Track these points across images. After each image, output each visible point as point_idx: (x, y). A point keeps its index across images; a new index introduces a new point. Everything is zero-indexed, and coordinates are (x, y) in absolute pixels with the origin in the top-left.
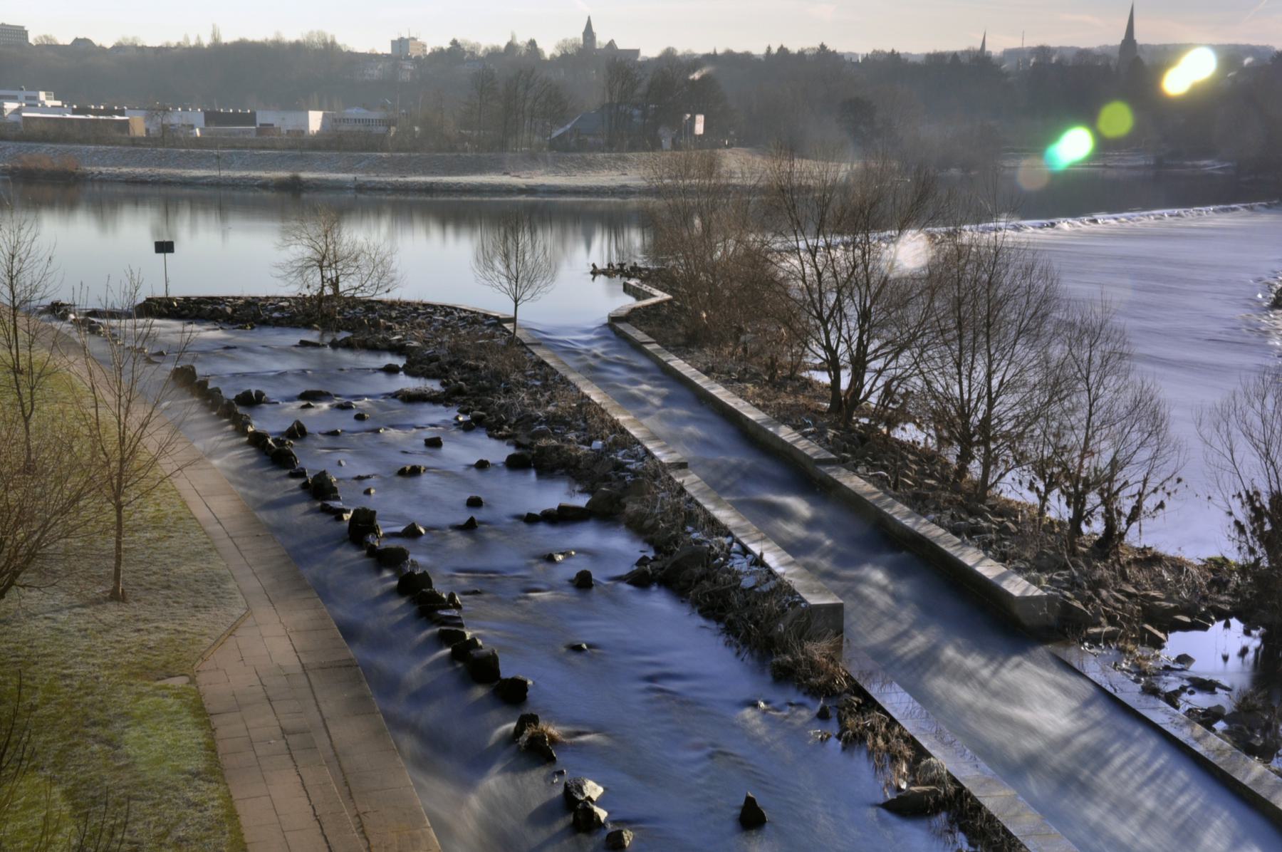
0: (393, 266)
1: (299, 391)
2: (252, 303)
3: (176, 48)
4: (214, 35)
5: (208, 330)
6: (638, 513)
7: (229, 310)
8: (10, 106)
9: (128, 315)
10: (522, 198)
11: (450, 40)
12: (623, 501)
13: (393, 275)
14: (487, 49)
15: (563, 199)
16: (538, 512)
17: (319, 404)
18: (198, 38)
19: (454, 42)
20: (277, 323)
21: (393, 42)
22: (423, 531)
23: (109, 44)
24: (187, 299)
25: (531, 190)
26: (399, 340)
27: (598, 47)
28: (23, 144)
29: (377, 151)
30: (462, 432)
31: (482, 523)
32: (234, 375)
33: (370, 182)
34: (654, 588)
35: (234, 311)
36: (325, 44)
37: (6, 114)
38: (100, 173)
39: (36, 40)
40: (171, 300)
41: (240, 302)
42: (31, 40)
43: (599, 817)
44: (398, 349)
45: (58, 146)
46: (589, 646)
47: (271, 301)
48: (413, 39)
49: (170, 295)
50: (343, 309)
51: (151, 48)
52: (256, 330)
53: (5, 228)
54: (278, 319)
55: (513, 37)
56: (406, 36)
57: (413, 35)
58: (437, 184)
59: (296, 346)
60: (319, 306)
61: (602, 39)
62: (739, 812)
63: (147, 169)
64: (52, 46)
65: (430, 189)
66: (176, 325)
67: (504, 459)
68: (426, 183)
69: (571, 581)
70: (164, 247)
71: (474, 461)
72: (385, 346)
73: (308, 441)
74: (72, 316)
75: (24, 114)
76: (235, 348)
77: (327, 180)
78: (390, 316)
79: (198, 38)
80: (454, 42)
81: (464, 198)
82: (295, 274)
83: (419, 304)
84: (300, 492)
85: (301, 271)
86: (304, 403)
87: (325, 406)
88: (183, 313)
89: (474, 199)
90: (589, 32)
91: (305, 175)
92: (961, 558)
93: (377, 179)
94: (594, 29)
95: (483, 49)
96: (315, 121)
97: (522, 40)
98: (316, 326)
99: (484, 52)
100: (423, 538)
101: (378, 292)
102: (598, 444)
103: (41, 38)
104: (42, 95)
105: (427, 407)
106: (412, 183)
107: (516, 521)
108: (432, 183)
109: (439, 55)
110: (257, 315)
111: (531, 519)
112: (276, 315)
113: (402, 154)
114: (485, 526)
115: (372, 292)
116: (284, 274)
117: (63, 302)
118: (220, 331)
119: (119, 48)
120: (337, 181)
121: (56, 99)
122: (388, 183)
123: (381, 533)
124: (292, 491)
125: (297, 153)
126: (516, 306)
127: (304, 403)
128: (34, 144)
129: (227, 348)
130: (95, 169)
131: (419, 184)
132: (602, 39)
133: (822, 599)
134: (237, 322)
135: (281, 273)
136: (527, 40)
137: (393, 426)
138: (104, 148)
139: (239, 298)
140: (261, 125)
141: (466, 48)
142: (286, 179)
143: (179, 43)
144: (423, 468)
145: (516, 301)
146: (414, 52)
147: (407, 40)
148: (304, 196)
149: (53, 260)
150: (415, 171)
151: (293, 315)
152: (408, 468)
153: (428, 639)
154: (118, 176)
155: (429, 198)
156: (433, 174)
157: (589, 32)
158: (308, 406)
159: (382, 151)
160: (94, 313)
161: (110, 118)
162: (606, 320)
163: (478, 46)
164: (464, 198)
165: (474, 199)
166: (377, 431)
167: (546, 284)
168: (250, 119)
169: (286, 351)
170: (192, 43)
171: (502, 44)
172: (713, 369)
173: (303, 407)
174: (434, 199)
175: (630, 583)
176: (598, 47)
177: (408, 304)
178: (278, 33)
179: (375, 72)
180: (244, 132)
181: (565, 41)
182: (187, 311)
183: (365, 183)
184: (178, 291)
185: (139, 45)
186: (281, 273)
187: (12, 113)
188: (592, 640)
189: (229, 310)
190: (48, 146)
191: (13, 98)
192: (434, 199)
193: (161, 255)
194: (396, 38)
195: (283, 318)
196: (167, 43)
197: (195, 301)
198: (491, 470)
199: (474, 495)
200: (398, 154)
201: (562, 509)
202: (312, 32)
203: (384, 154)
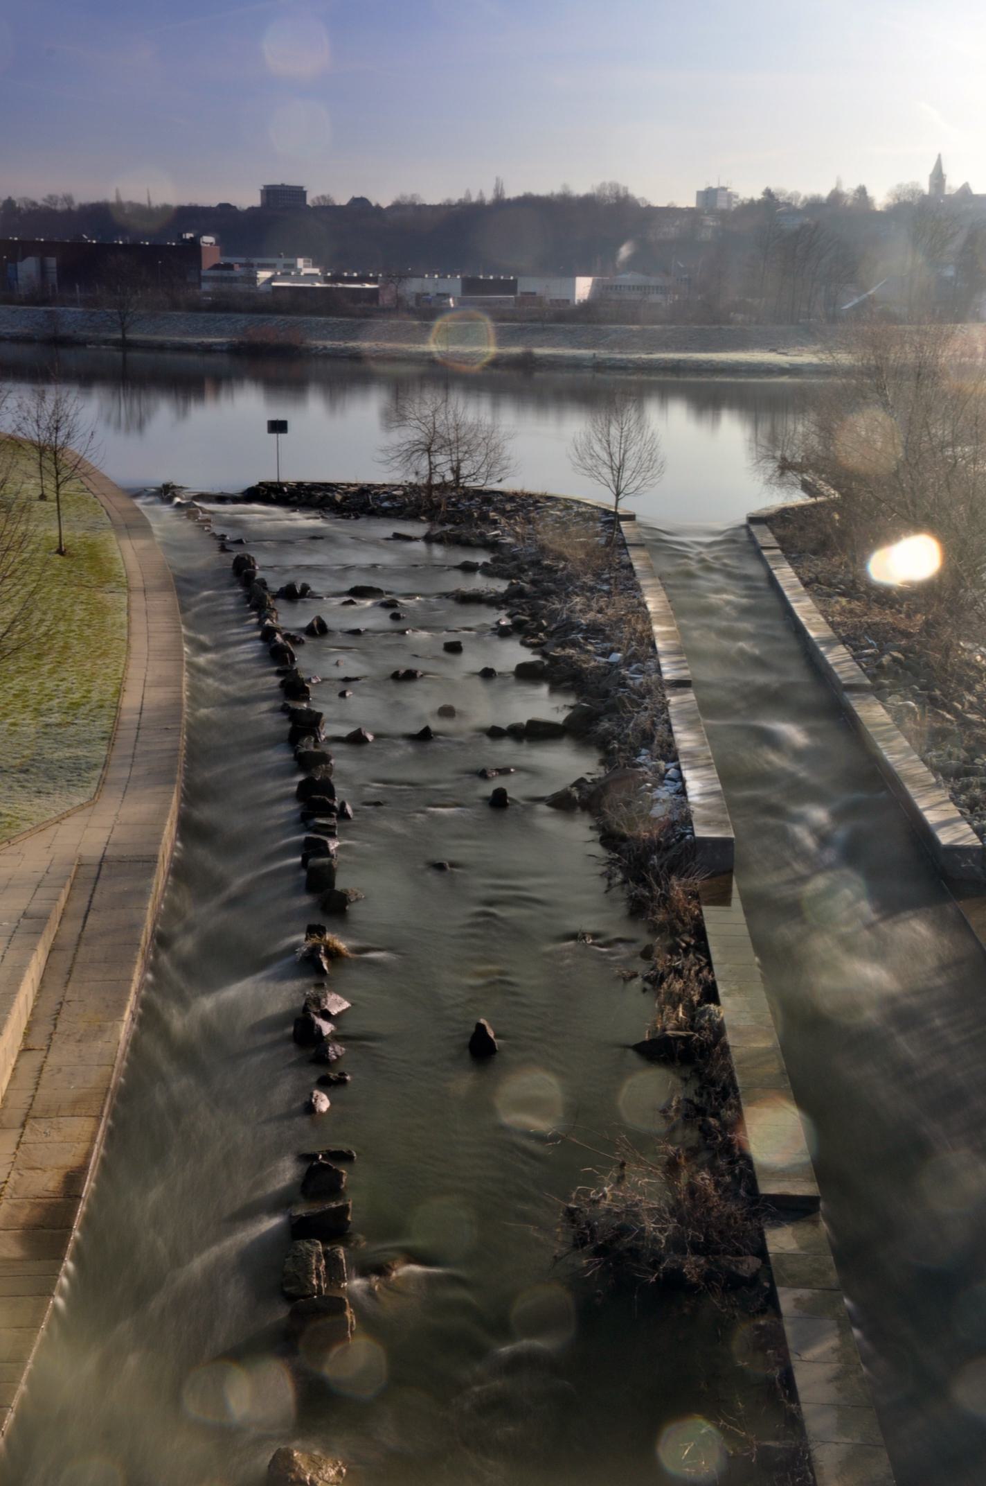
0: (506, 453)
1: (347, 587)
2: (365, 490)
3: (456, 206)
4: (496, 190)
5: (308, 518)
6: (608, 733)
7: (338, 498)
8: (264, 275)
9: (235, 499)
10: (785, 379)
11: (763, 189)
12: (601, 718)
13: (504, 463)
14: (806, 199)
15: (719, 379)
16: (505, 726)
17: (362, 602)
18: (481, 193)
19: (768, 193)
20: (385, 514)
21: (699, 193)
22: (370, 737)
23: (385, 202)
24: (300, 484)
25: (794, 370)
26: (497, 536)
27: (947, 192)
28: (255, 316)
29: (628, 323)
30: (497, 637)
31: (437, 734)
32: (298, 567)
33: (610, 359)
34: (579, 810)
35: (345, 499)
36: (618, 197)
37: (258, 284)
38: (325, 348)
39: (313, 201)
40: (281, 485)
41: (352, 489)
42: (309, 202)
43: (320, 1030)
44: (491, 546)
45: (289, 318)
46: (453, 865)
47: (386, 490)
48: (724, 189)
49: (282, 480)
50: (458, 501)
51: (430, 206)
52: (360, 520)
53: (11, 402)
54: (387, 509)
55: (839, 183)
56: (715, 186)
57: (723, 184)
58: (685, 361)
59: (388, 539)
60: (430, 495)
61: (953, 183)
62: (468, 1040)
63: (373, 344)
64: (328, 207)
65: (676, 368)
66: (277, 511)
67: (513, 668)
68: (672, 360)
69: (486, 798)
70: (278, 427)
71: (479, 668)
72: (479, 542)
73: (328, 641)
74: (177, 500)
75: (274, 284)
76: (321, 538)
77: (561, 357)
78: (504, 509)
79: (481, 193)
80: (768, 193)
81: (718, 379)
82: (400, 459)
83: (541, 496)
84: (279, 690)
85: (409, 454)
86: (347, 599)
87: (369, 603)
88: (291, 499)
89: (728, 380)
90: (938, 177)
91: (538, 351)
92: (916, 800)
93: (619, 356)
94: (945, 171)
95: (802, 198)
96: (583, 287)
97: (849, 187)
98: (423, 518)
99: (803, 203)
100: (367, 747)
101: (489, 482)
102: (616, 657)
103: (318, 198)
104: (300, 262)
105: (483, 608)
106: (657, 360)
107: (478, 734)
108: (680, 361)
109: (750, 208)
110: (367, 504)
111: (495, 733)
112: (386, 504)
113: (656, 327)
114: (440, 737)
115: (483, 482)
116: (385, 458)
117: (175, 484)
118: (321, 520)
119: (397, 207)
120: (574, 358)
121: (314, 266)
122: (630, 361)
123: (323, 737)
124: (270, 689)
125: (538, 325)
126: (617, 500)
127: (347, 599)
128: (266, 316)
129: (314, 538)
130: (320, 343)
131: (665, 361)
132: (953, 183)
133: (710, 832)
134: (349, 510)
135: (383, 457)
136: (855, 186)
137: (423, 628)
138: (335, 319)
139: (351, 485)
140: (522, 293)
141: (781, 199)
142: (518, 355)
143: (460, 200)
144: (419, 674)
145: (618, 494)
146: (722, 204)
147: (716, 190)
148: (537, 375)
149: (95, 435)
150: (667, 347)
151: (404, 505)
152: (402, 671)
153: (297, 843)
154: (343, 351)
155: (675, 379)
156: (687, 350)
157: (938, 177)
158: (351, 602)
159: (633, 323)
160: (203, 497)
161: (334, 286)
162: (744, 521)
163: (798, 195)
164: (718, 379)
165: (728, 380)
166: (403, 632)
167: (653, 477)
168: (510, 287)
169: (374, 542)
170: (474, 199)
171: (824, 192)
172: (817, 580)
173: (345, 603)
174: (681, 379)
175: (550, 805)
176: (947, 192)
177: (530, 496)
178: (565, 186)
179: (671, 231)
180: (501, 301)
181: (899, 186)
182: (296, 498)
183: (604, 361)
184: (292, 474)
185: (418, 203)
186: (383, 457)
187: (264, 283)
188: (452, 858)
189: (338, 498)
190: (281, 317)
191: (264, 267)
192: (681, 379)
193: (274, 435)
194: (702, 188)
195: (393, 508)
196: (449, 200)
197: (307, 487)
198: (497, 682)
199: (449, 703)
200: (650, 327)
201: (533, 724)
202: (603, 184)
203: (635, 327)
